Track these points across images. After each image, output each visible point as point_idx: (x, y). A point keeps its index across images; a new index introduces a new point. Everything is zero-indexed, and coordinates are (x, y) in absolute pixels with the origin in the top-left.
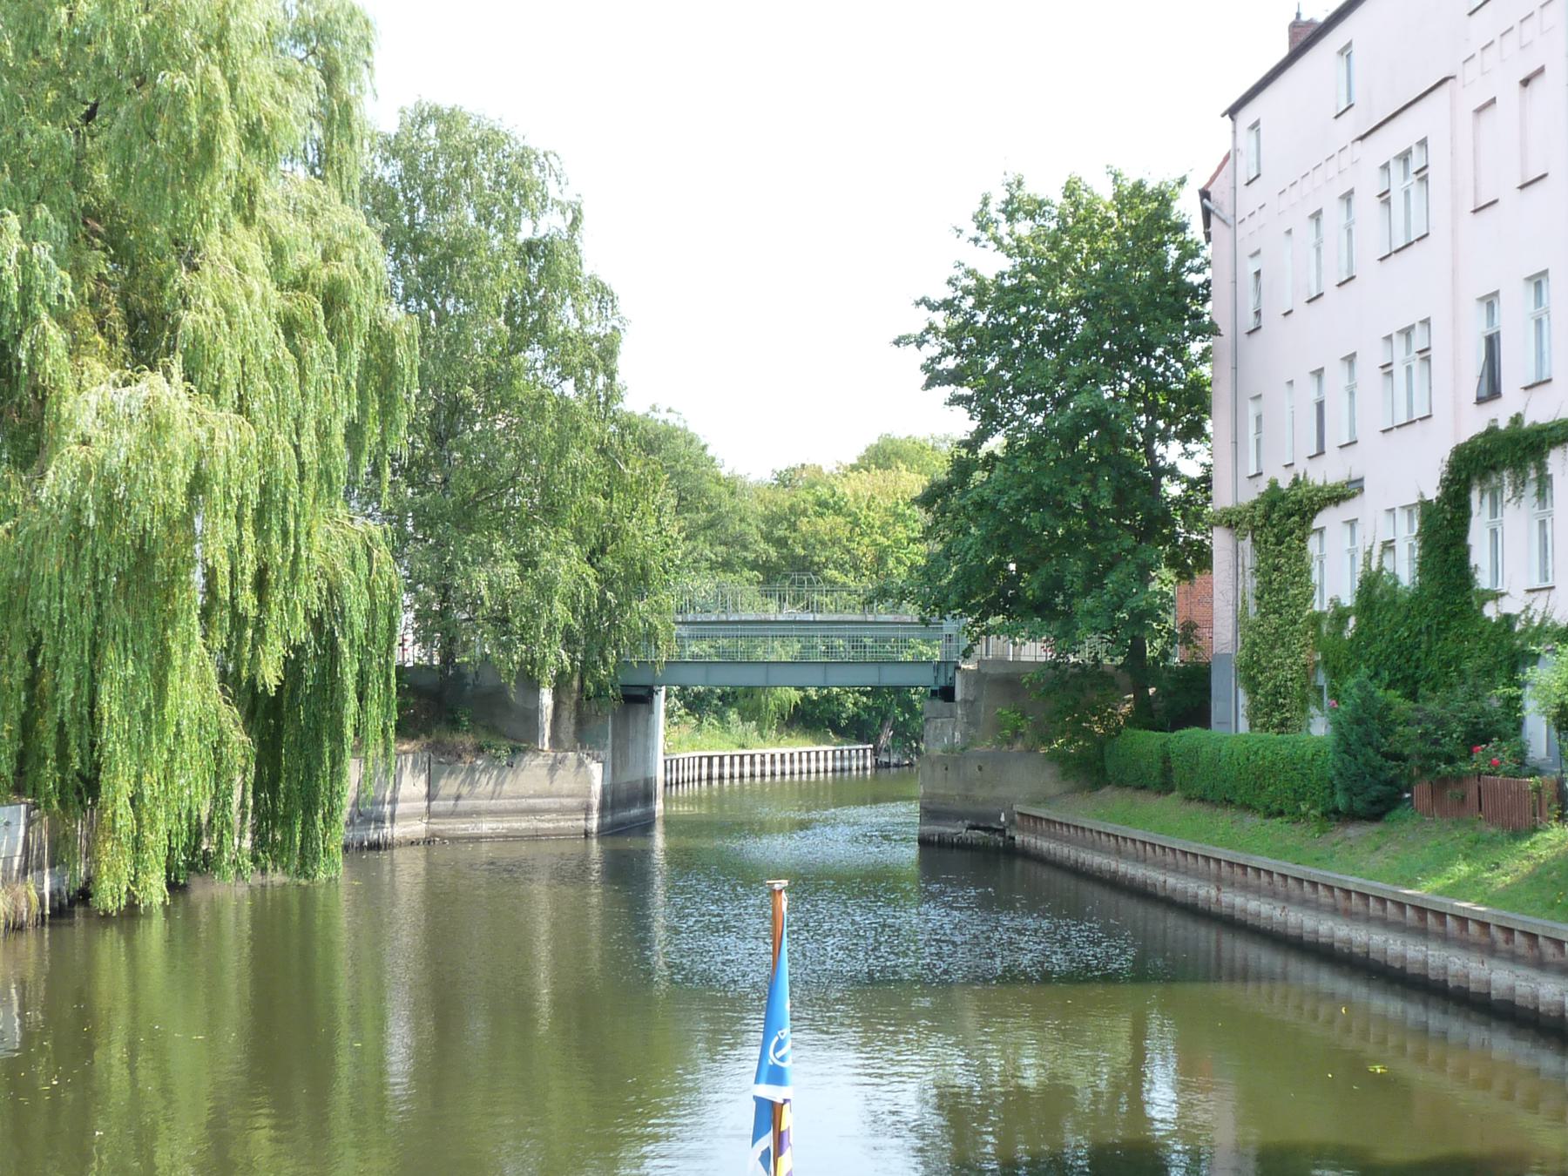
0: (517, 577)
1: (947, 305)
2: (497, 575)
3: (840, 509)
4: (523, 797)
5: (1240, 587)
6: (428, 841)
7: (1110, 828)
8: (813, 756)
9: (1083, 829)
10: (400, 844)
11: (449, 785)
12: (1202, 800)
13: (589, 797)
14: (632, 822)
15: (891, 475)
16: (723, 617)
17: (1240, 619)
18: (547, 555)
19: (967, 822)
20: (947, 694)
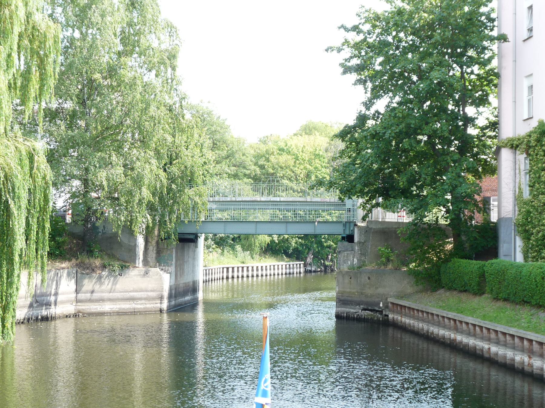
0: (123, 175)
1: (355, 28)
2: (112, 174)
3: (290, 152)
4: (127, 292)
5: (517, 181)
6: (75, 316)
7: (451, 315)
8: (276, 267)
9: (432, 314)
10: (60, 317)
11: (88, 284)
12: (505, 300)
13: (162, 291)
14: (186, 304)
15: (312, 137)
16: (234, 199)
17: (518, 198)
18: (138, 164)
19: (362, 306)
20: (350, 238)
